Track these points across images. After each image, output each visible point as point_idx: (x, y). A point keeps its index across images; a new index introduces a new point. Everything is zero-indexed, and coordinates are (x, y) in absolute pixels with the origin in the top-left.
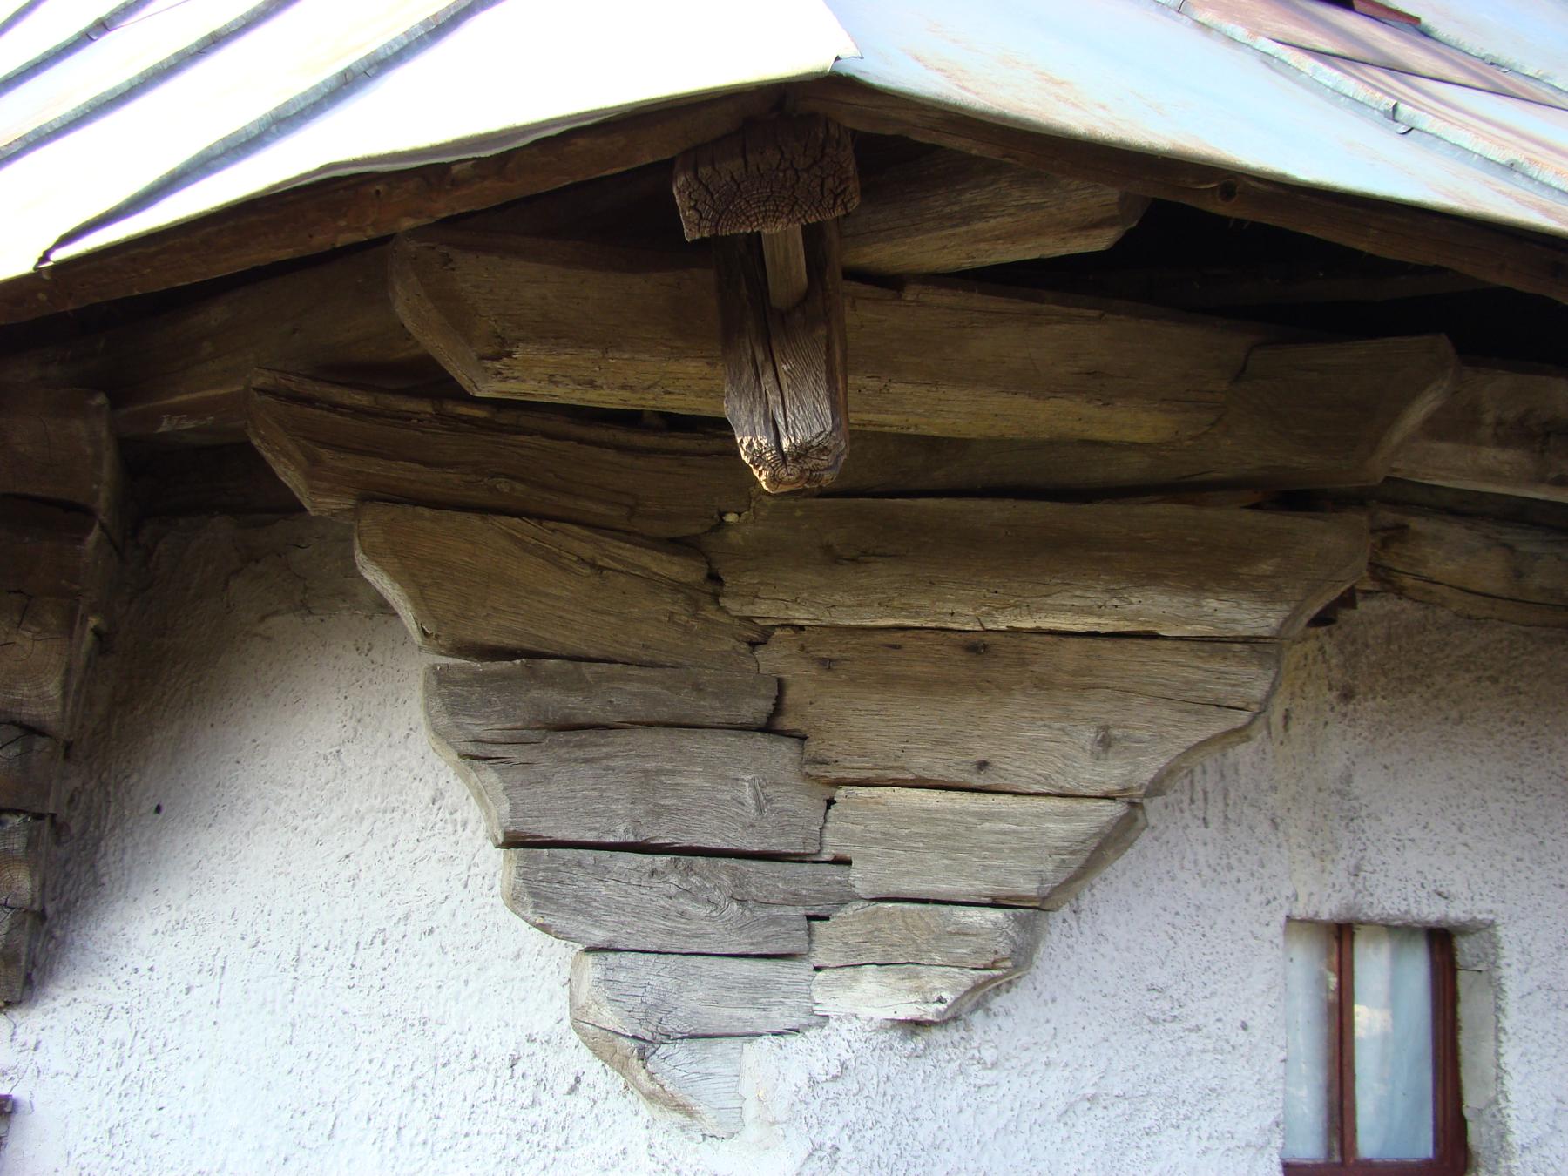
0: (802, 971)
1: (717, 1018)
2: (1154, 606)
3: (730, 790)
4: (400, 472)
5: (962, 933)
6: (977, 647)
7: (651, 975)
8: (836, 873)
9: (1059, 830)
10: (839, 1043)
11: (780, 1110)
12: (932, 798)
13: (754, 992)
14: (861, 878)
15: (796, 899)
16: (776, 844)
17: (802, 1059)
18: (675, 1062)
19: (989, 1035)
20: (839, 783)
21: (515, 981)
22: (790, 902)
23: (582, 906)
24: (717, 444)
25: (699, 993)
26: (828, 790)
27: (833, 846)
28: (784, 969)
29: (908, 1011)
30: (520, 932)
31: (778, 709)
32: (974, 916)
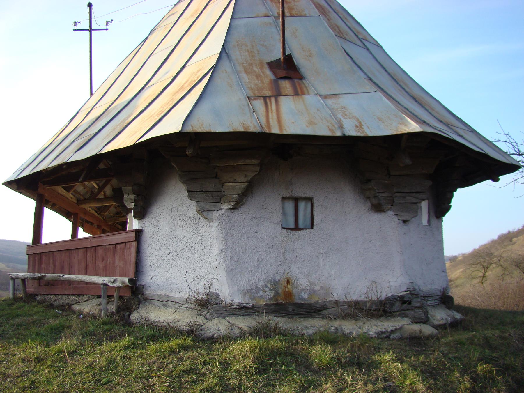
0: (220, 204)
1: (210, 209)
2: (248, 161)
3: (211, 185)
4: (188, 83)
5: (233, 198)
6: (234, 167)
7: (203, 205)
8: (223, 193)
9: (243, 186)
10: (223, 211)
11: (216, 218)
12: (231, 184)
13: (214, 206)
14: (226, 193)
15: (219, 196)
16: (216, 190)
17: (220, 212)
18: (205, 213)
19: (241, 210)
20: (224, 183)
21: (191, 208)
22: (218, 197)
23: (195, 198)
24: (36, 270)
25: (208, 206)
26: (223, 184)
27: (223, 190)
28: (218, 204)
29: (230, 207)
30: (189, 201)
31: (217, 175)
32: (235, 196)
